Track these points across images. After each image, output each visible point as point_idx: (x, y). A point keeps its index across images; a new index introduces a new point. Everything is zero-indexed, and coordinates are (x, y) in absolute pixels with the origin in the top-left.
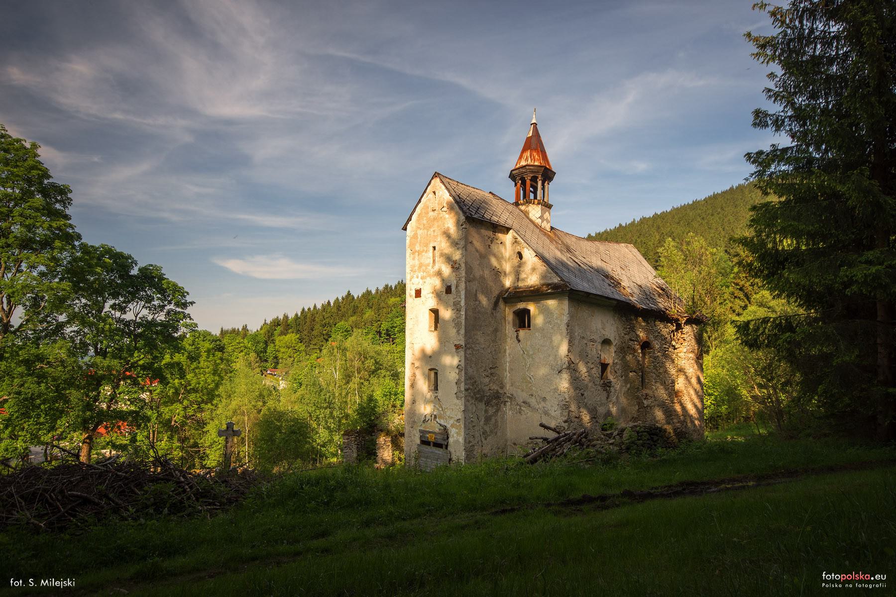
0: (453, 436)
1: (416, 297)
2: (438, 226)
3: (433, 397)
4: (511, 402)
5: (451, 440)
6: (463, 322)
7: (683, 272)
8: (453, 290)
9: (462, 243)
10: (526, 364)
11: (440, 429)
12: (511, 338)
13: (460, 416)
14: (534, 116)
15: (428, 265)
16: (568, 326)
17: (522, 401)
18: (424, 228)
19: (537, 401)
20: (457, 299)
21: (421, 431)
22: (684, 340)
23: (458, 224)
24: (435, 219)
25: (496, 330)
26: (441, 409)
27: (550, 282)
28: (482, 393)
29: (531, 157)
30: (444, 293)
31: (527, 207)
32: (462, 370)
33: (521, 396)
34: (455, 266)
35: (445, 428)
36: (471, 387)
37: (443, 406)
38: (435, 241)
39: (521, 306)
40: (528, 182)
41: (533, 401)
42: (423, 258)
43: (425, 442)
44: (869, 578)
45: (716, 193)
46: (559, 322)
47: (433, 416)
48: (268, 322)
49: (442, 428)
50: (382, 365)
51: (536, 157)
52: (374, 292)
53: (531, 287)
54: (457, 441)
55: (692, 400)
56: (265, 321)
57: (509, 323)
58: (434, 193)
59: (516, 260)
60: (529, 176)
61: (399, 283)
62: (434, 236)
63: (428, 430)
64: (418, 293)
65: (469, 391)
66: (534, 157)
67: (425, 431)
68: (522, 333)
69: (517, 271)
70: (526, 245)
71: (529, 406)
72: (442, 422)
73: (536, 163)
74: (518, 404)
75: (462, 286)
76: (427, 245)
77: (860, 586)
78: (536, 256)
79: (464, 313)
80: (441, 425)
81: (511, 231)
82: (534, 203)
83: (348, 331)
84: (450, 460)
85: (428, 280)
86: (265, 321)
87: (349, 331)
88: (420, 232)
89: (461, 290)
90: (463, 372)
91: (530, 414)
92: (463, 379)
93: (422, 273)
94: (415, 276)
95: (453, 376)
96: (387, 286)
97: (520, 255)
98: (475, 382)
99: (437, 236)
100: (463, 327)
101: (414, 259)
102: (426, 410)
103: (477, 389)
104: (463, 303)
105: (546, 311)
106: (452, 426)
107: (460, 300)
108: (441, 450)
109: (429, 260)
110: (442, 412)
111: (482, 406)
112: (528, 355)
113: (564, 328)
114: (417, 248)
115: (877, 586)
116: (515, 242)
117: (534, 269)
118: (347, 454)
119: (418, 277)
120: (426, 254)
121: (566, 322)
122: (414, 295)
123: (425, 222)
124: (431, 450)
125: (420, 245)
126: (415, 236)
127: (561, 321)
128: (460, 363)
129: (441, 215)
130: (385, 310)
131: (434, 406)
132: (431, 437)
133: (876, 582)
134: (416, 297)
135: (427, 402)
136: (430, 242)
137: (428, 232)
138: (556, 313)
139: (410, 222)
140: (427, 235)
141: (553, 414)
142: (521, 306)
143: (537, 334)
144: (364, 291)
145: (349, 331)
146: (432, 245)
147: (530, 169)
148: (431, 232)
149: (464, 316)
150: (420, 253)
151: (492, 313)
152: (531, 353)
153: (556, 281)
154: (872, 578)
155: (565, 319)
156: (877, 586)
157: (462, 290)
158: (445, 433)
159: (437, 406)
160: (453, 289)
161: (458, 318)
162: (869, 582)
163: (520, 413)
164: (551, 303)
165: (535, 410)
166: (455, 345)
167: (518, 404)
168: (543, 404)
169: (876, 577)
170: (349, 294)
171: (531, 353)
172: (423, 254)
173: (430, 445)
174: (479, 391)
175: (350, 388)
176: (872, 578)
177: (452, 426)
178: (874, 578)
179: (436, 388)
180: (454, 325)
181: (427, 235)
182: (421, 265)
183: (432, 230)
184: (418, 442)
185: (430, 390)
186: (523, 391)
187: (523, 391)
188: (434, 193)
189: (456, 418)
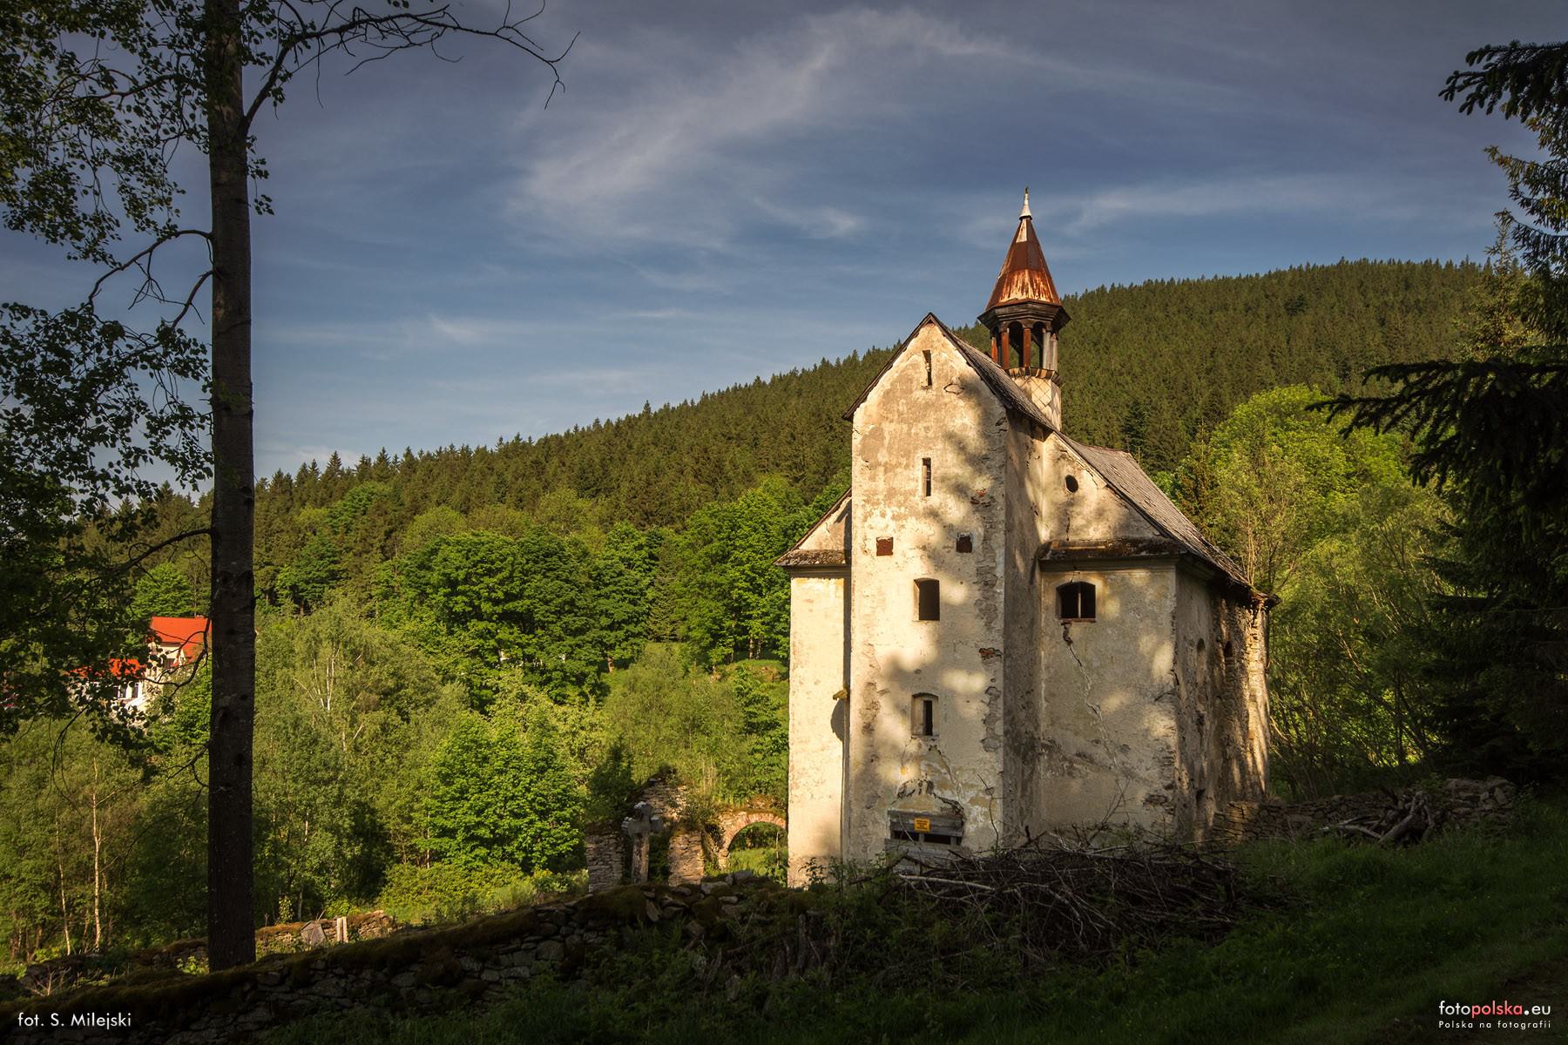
1: (878, 554)
2: (937, 420)
3: (925, 748)
4: (1050, 755)
5: (970, 828)
6: (1001, 608)
7: (39, 359)
8: (974, 545)
10: (1084, 685)
12: (1052, 636)
14: (1026, 202)
15: (913, 493)
16: (1174, 617)
18: (902, 421)
19: (1108, 753)
20: (985, 564)
22: (1255, 638)
23: (985, 419)
24: (928, 405)
27: (1137, 536)
29: (1032, 286)
30: (953, 551)
32: (999, 697)
33: (1074, 742)
34: (979, 503)
38: (931, 449)
39: (1072, 577)
40: (1027, 333)
41: (1099, 753)
42: (899, 477)
44: (1521, 1012)
47: (925, 784)
49: (949, 806)
50: (403, 678)
51: (1042, 285)
53: (1097, 544)
55: (1260, 747)
58: (927, 355)
59: (1062, 495)
60: (1030, 322)
63: (911, 810)
64: (885, 547)
66: (1038, 286)
67: (906, 814)
68: (1077, 629)
69: (1064, 515)
70: (1084, 464)
71: (1092, 761)
72: (948, 795)
73: (1043, 299)
74: (1065, 759)
75: (999, 538)
76: (907, 454)
77: (1505, 1025)
78: (1107, 486)
79: (1003, 590)
80: (945, 801)
81: (1052, 436)
82: (1039, 377)
83: (181, 589)
85: (912, 523)
87: (185, 588)
88: (888, 428)
89: (995, 546)
90: (1000, 701)
91: (1092, 775)
92: (1000, 713)
94: (877, 512)
95: (974, 711)
96: (279, 474)
97: (1072, 484)
100: (1001, 616)
101: (873, 478)
102: (902, 775)
105: (1126, 593)
106: (973, 801)
110: (948, 777)
112: (1088, 668)
113: (1165, 620)
114: (883, 457)
115: (1535, 1026)
116: (1061, 457)
117: (1100, 514)
118: (599, 873)
119: (883, 515)
120: (905, 473)
121: (1170, 610)
122: (874, 549)
125: (890, 453)
126: (877, 434)
127: (1160, 608)
128: (993, 684)
129: (947, 400)
130: (285, 537)
131: (929, 765)
133: (1532, 1018)
134: (878, 554)
135: (903, 758)
136: (916, 448)
137: (910, 429)
138: (1150, 594)
140: (909, 434)
141: (1143, 774)
142: (1072, 577)
145: (185, 588)
146: (921, 454)
147: (1035, 309)
148: (919, 429)
150: (888, 468)
152: (1096, 664)
153: (1151, 536)
154: (1527, 1013)
155: (1170, 604)
156: (1535, 1026)
158: (956, 815)
159: (935, 765)
160: (976, 543)
161: (987, 599)
162: (1522, 1018)
164: (1139, 576)
165: (1102, 768)
166: (981, 651)
167: (1065, 759)
168: (1122, 757)
169: (1533, 1010)
171: (1096, 664)
172: (899, 470)
173: (949, 843)
175: (362, 734)
176: (1527, 1013)
177: (973, 801)
178: (1530, 1012)
179: (927, 728)
180: (977, 612)
181: (909, 434)
182: (891, 494)
184: (887, 834)
185: (915, 735)
186: (1076, 734)
187: (1076, 734)
188: (927, 355)
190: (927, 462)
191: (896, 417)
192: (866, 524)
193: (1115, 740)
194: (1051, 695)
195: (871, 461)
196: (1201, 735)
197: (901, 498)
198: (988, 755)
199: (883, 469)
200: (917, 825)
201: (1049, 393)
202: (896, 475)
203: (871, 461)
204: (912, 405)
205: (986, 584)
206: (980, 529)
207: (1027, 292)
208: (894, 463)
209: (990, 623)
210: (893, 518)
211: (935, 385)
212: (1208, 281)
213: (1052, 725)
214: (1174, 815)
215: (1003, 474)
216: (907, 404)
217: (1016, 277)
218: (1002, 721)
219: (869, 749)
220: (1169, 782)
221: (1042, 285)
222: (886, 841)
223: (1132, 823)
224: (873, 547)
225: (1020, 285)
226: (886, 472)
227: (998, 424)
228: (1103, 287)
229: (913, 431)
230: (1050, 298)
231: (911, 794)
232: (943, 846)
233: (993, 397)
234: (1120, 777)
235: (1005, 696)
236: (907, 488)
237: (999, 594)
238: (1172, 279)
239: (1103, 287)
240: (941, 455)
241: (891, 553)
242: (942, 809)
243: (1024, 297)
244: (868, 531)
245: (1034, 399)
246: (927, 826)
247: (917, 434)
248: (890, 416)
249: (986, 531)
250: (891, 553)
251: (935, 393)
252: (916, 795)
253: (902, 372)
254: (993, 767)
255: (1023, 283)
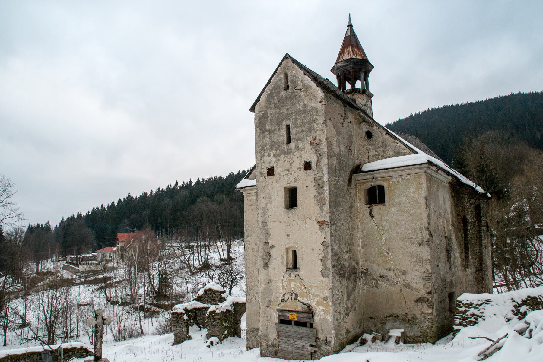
0: (319, 314)
5: (316, 318)
6: (327, 198)
9: (321, 119)
10: (381, 239)
11: (302, 308)
13: (327, 293)
17: (378, 275)
18: (276, 107)
19: (395, 275)
21: (279, 310)
25: (351, 207)
26: (303, 287)
28: (344, 270)
29: (353, 52)
30: (303, 170)
31: (354, 95)
32: (328, 247)
35: (309, 306)
36: (336, 264)
37: (306, 285)
38: (289, 119)
41: (390, 274)
42: (276, 136)
43: (284, 321)
45: (401, 119)
46: (417, 195)
48: (65, 219)
51: (358, 52)
52: (149, 194)
54: (325, 319)
56: (63, 217)
57: (360, 200)
61: (168, 187)
62: (288, 114)
65: (335, 268)
66: (356, 52)
68: (377, 209)
71: (387, 280)
72: (305, 300)
73: (358, 57)
74: (373, 279)
75: (325, 161)
76: (279, 124)
80: (303, 304)
84: (317, 338)
86: (63, 217)
88: (270, 112)
90: (329, 250)
92: (329, 256)
93: (274, 151)
94: (267, 154)
98: (339, 259)
99: (292, 113)
103: (341, 265)
104: (326, 179)
106: (318, 304)
107: (321, 175)
108: (306, 329)
109: (282, 138)
111: (344, 281)
114: (268, 126)
119: (269, 155)
123: (276, 101)
124: (292, 330)
125: (271, 125)
129: (296, 94)
132: (293, 317)
136: (283, 120)
137: (280, 111)
139: (258, 103)
140: (279, 114)
141: (415, 286)
143: (393, 209)
144: (142, 193)
146: (285, 123)
149: (328, 192)
150: (271, 131)
151: (348, 190)
152: (387, 227)
157: (325, 166)
158: (310, 311)
160: (313, 165)
163: (376, 287)
166: (318, 222)
168: (403, 277)
170: (129, 195)
171: (387, 227)
172: (276, 132)
174: (342, 267)
177: (318, 304)
181: (279, 114)
182: (272, 144)
183: (285, 108)
187: (379, 265)
189: (323, 296)
190: (288, 128)
191: (273, 106)
192: (262, 161)
193: (399, 268)
194: (364, 245)
195: (263, 129)
196: (450, 263)
197: (277, 146)
198: (324, 279)
199: (268, 132)
200: (290, 317)
201: (365, 100)
202: (274, 135)
203: (263, 129)
204: (281, 99)
205: (319, 186)
206: (315, 157)
207: (351, 55)
208: (273, 129)
209: (322, 206)
210: (274, 156)
211: (290, 87)
212: (465, 104)
213: (366, 261)
214: (433, 308)
215: (325, 127)
216: (278, 99)
217: (345, 50)
218: (330, 260)
219: (266, 277)
220: (429, 290)
221: (358, 52)
222: (276, 324)
223: (410, 313)
224: (265, 172)
225: (347, 53)
226: (270, 133)
227: (321, 102)
228: (428, 109)
229: (281, 112)
230: (362, 57)
231: (287, 300)
232: (303, 328)
233: (317, 88)
234: (403, 288)
235: (332, 245)
236: (280, 141)
237: (326, 190)
238: (452, 104)
239: (428, 109)
240: (295, 122)
241: (273, 175)
242: (302, 308)
243: (349, 57)
244: (263, 164)
245: (357, 102)
246: (295, 317)
247: (283, 113)
248: (271, 106)
249: (318, 158)
250: (273, 175)
251: (290, 91)
252: (289, 300)
253: (275, 84)
254: (327, 285)
255: (349, 52)
